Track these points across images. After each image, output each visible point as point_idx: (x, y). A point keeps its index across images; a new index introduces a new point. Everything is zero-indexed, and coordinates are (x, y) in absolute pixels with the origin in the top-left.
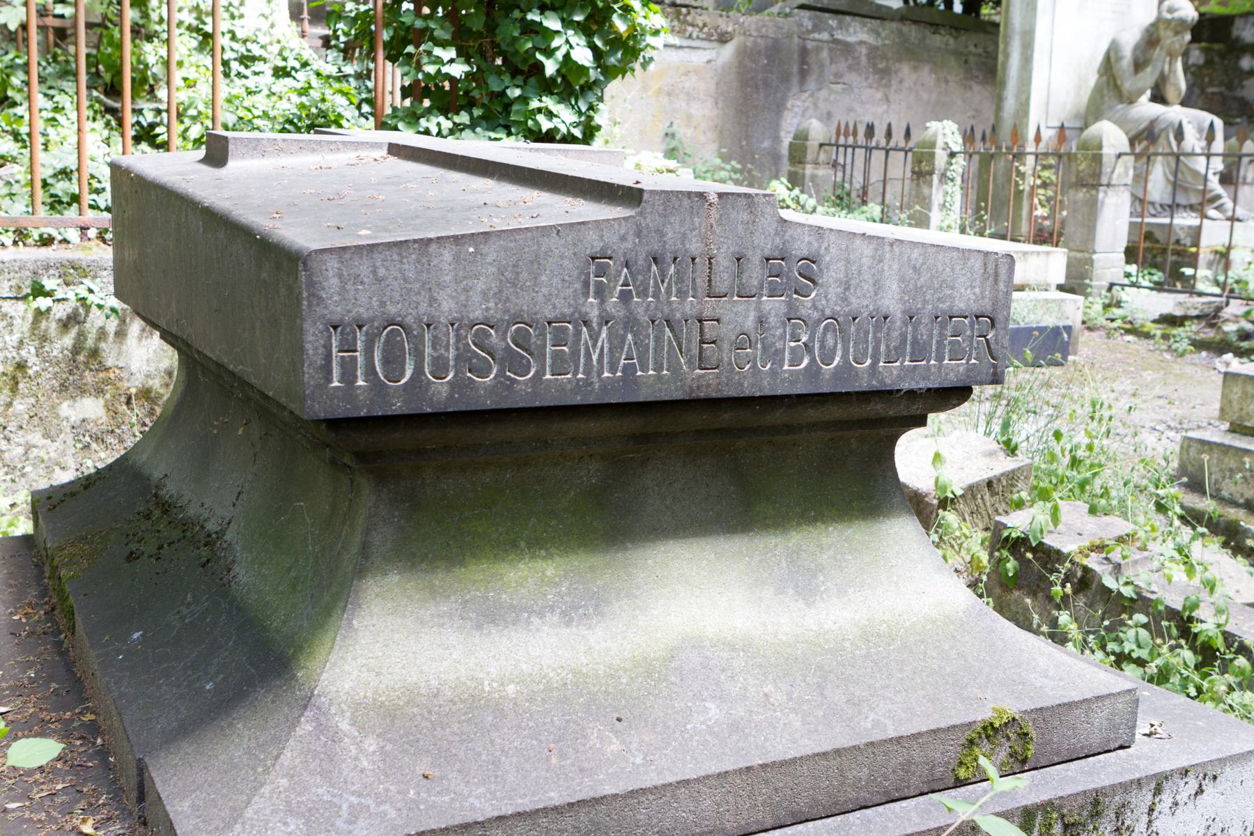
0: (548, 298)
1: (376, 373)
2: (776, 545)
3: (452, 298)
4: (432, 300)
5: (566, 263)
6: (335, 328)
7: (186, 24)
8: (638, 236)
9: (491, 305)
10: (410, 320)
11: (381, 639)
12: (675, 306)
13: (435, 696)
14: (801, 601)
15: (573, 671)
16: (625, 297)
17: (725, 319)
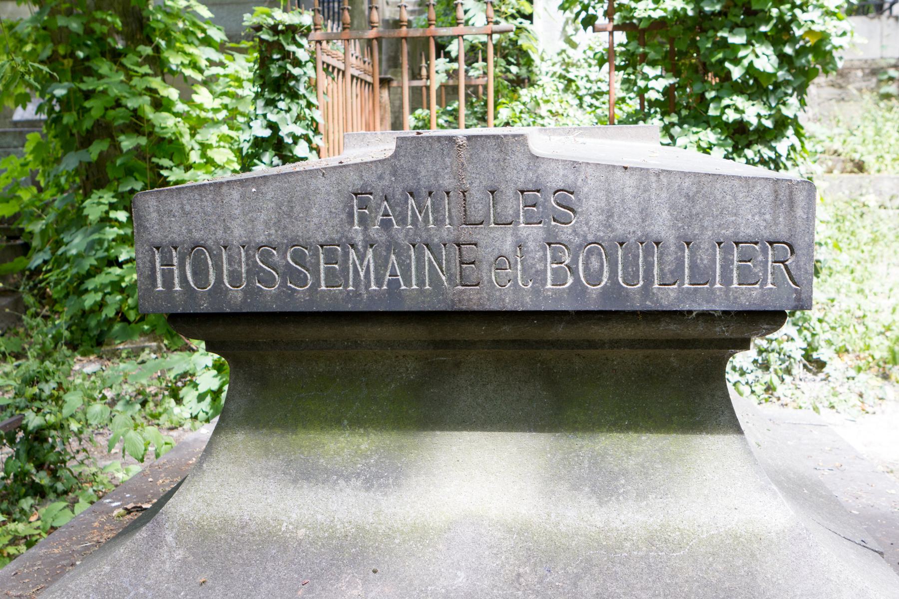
0: (319, 226)
1: (187, 282)
2: (582, 447)
3: (242, 226)
4: (226, 229)
5: (332, 198)
6: (158, 248)
7: (558, 74)
8: (394, 175)
9: (273, 231)
10: (210, 243)
11: (219, 480)
12: (432, 232)
13: (243, 528)
14: (594, 499)
15: (358, 528)
16: (386, 225)
17: (482, 243)
